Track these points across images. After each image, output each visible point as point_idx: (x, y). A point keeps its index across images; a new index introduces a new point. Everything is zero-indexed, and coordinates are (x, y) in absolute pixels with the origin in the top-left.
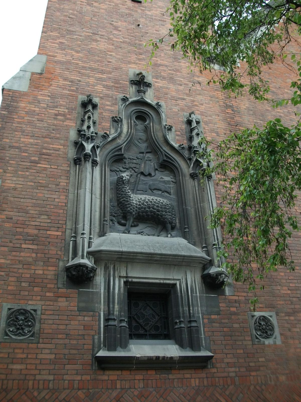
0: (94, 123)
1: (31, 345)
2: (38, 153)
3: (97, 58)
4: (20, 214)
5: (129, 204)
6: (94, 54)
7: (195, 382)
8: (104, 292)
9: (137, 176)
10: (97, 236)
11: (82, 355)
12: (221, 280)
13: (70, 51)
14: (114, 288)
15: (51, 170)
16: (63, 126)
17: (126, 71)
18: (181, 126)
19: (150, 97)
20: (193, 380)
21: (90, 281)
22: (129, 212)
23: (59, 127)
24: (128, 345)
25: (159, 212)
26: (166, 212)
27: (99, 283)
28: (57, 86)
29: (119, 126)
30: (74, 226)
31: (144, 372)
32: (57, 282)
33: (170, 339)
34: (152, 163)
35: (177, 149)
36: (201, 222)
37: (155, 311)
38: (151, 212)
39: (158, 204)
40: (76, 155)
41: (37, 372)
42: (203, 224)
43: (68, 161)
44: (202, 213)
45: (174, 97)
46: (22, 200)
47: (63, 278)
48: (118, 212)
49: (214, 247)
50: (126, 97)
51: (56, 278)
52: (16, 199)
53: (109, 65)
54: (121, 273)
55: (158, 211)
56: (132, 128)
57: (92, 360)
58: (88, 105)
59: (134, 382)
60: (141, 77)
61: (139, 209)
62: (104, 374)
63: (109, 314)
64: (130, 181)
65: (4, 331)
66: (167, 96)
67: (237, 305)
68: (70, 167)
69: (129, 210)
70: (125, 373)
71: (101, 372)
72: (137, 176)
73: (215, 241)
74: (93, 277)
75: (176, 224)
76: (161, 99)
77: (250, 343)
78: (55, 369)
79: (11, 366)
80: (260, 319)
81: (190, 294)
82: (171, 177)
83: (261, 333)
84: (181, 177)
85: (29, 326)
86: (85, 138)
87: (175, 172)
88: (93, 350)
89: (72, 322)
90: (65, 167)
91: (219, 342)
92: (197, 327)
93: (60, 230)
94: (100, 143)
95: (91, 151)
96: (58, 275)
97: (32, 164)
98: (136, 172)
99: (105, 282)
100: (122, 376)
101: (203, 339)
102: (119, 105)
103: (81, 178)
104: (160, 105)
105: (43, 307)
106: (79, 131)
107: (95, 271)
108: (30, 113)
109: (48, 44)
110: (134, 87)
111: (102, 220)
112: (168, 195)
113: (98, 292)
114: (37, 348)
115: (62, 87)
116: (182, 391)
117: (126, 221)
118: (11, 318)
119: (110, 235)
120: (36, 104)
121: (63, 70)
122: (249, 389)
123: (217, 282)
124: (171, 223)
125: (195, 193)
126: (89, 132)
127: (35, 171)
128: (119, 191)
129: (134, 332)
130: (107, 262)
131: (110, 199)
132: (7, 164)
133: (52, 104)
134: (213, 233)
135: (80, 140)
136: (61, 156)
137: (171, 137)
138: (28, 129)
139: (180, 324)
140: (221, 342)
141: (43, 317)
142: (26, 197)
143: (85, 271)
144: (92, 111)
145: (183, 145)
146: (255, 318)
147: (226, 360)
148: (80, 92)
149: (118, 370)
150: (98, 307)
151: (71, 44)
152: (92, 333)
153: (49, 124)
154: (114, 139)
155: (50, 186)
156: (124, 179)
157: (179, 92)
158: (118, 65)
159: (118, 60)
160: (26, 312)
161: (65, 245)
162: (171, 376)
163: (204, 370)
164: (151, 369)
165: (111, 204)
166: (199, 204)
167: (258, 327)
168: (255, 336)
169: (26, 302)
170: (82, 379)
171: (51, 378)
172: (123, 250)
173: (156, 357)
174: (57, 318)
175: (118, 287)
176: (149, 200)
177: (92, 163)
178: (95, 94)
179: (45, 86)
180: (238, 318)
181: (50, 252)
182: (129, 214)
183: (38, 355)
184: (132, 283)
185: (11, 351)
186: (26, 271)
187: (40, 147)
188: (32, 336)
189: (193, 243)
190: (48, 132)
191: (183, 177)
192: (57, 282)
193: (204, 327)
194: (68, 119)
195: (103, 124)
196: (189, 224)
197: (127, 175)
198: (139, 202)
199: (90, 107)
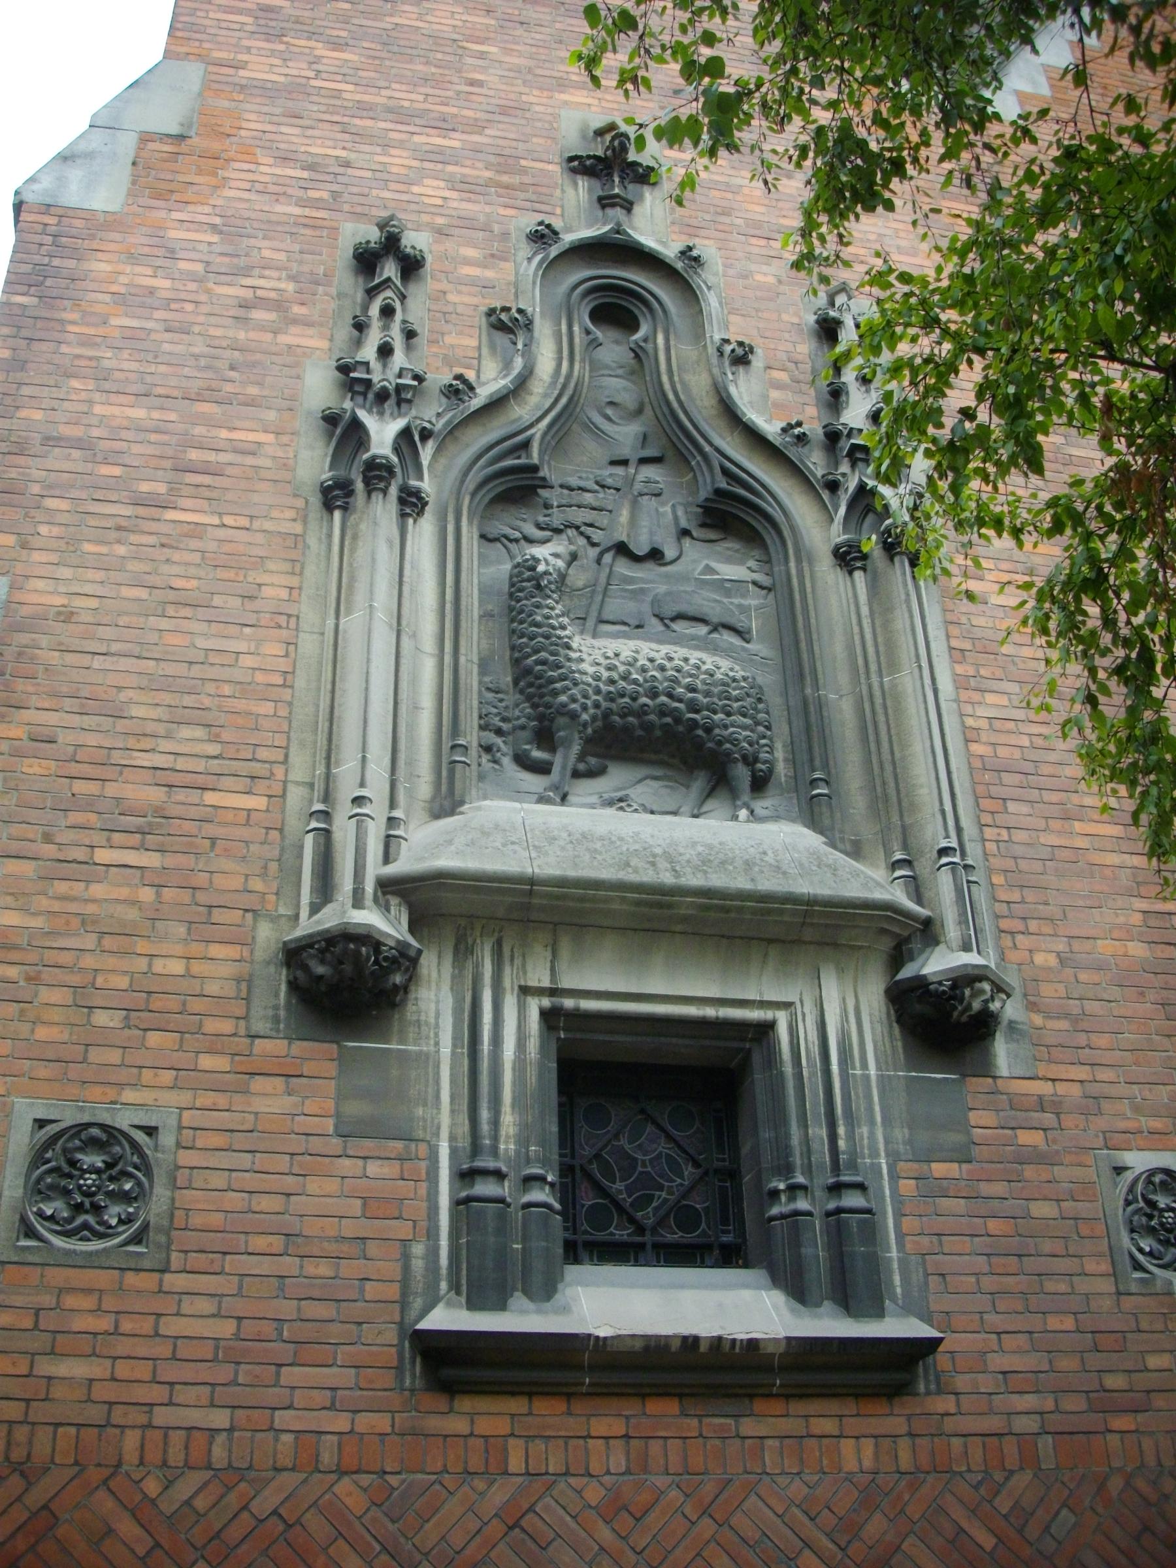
0: (410, 335)
1: (131, 1278)
2: (168, 464)
3: (420, 67)
4: (87, 721)
5: (563, 678)
6: (409, 51)
7: (859, 1451)
8: (453, 1053)
9: (598, 561)
10: (424, 816)
11: (353, 1327)
12: (976, 1005)
13: (303, 43)
14: (497, 1040)
15: (222, 533)
16: (274, 349)
17: (549, 118)
18: (790, 347)
19: (652, 225)
20: (847, 1445)
21: (393, 1005)
22: (562, 710)
23: (258, 356)
24: (560, 1286)
25: (697, 712)
26: (729, 714)
27: (432, 1014)
28: (247, 186)
29: (520, 346)
30: (320, 770)
31: (630, 1407)
32: (248, 1009)
33: (746, 1265)
34: (663, 504)
35: (777, 441)
36: (886, 756)
37: (679, 1146)
38: (663, 711)
39: (691, 676)
40: (330, 469)
41: (157, 1393)
42: (894, 763)
43: (295, 495)
44: (886, 714)
45: (757, 224)
46: (98, 662)
47: (276, 988)
48: (517, 713)
49: (944, 860)
50: (548, 226)
51: (244, 994)
52: (70, 658)
53: (474, 97)
54: (529, 975)
55: (694, 707)
56: (577, 358)
57: (400, 1345)
58: (385, 261)
59: (586, 1449)
60: (613, 139)
61: (610, 697)
62: (451, 1411)
63: (476, 1149)
64: (568, 581)
65: (18, 1217)
66: (726, 220)
67: (1048, 1118)
68: (305, 522)
69: (564, 705)
70: (542, 1406)
71: (442, 1402)
72: (598, 561)
73: (947, 837)
74: (406, 989)
75: (771, 764)
76: (702, 232)
77: (1107, 1286)
78: (234, 1383)
79: (46, 1367)
80: (1149, 1181)
81: (835, 1068)
82: (752, 563)
83: (1157, 1246)
84: (792, 564)
85: (126, 1198)
86: (370, 396)
87: (769, 542)
88: (404, 1304)
89: (313, 1185)
90: (284, 521)
91: (963, 1278)
92: (869, 1211)
93: (261, 787)
94: (434, 420)
95: (397, 449)
96: (250, 982)
97: (141, 511)
98: (594, 545)
99: (457, 1011)
100: (530, 1418)
101: (895, 1266)
102: (519, 259)
103: (351, 565)
104: (696, 259)
105: (186, 1114)
106: (344, 369)
107: (414, 961)
108: (137, 299)
109: (211, 15)
110: (583, 183)
111: (446, 746)
112: (736, 641)
113: (427, 1055)
114: (160, 1291)
115: (272, 188)
116: (797, 1489)
117: (553, 750)
118: (48, 1161)
119: (479, 808)
120: (159, 262)
121: (275, 119)
122: (1102, 1487)
123: (955, 1014)
124: (750, 761)
125: (856, 629)
126: (388, 371)
127: (152, 540)
128: (521, 622)
129: (586, 1232)
130: (463, 922)
131: (480, 659)
132: (33, 512)
133: (227, 260)
134: (937, 804)
135: (348, 405)
136: (264, 474)
137: (745, 392)
138: (126, 365)
139: (792, 1199)
140: (973, 1279)
141: (186, 1158)
142: (115, 647)
143: (368, 959)
144: (398, 283)
145: (799, 424)
146: (1129, 1176)
147: (998, 1361)
148: (346, 207)
149: (513, 1394)
150: (425, 1120)
151: (307, 14)
152: (402, 1230)
153: (213, 343)
154: (497, 404)
155: (217, 601)
156: (541, 568)
157: (780, 204)
158: (512, 96)
159: (511, 74)
160: (112, 1134)
161: (282, 849)
162: (748, 1426)
163: (896, 1400)
164: (663, 1392)
165: (487, 679)
166: (875, 679)
167: (1144, 1219)
168: (1127, 1257)
169: (111, 1093)
170: (357, 1429)
171: (220, 1419)
172: (537, 871)
173: (685, 1338)
174: (248, 1166)
175: (517, 1037)
176: (651, 660)
177: (402, 501)
178: (414, 217)
179: (195, 188)
180: (1051, 1178)
181: (218, 880)
182: (562, 721)
183: (163, 1319)
184: (580, 1018)
185: (48, 1300)
186: (111, 962)
187: (174, 440)
188: (137, 1239)
189: (848, 847)
190: (210, 374)
191: (805, 564)
192: (248, 1009)
193: (899, 1215)
194: (295, 321)
195: (449, 340)
196: (831, 762)
197: (556, 555)
198: (610, 668)
199: (390, 270)
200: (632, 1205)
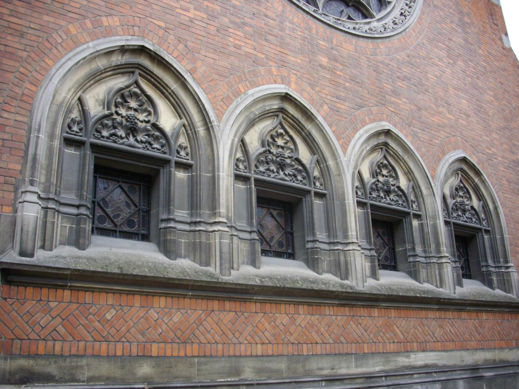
200: (113, 216)
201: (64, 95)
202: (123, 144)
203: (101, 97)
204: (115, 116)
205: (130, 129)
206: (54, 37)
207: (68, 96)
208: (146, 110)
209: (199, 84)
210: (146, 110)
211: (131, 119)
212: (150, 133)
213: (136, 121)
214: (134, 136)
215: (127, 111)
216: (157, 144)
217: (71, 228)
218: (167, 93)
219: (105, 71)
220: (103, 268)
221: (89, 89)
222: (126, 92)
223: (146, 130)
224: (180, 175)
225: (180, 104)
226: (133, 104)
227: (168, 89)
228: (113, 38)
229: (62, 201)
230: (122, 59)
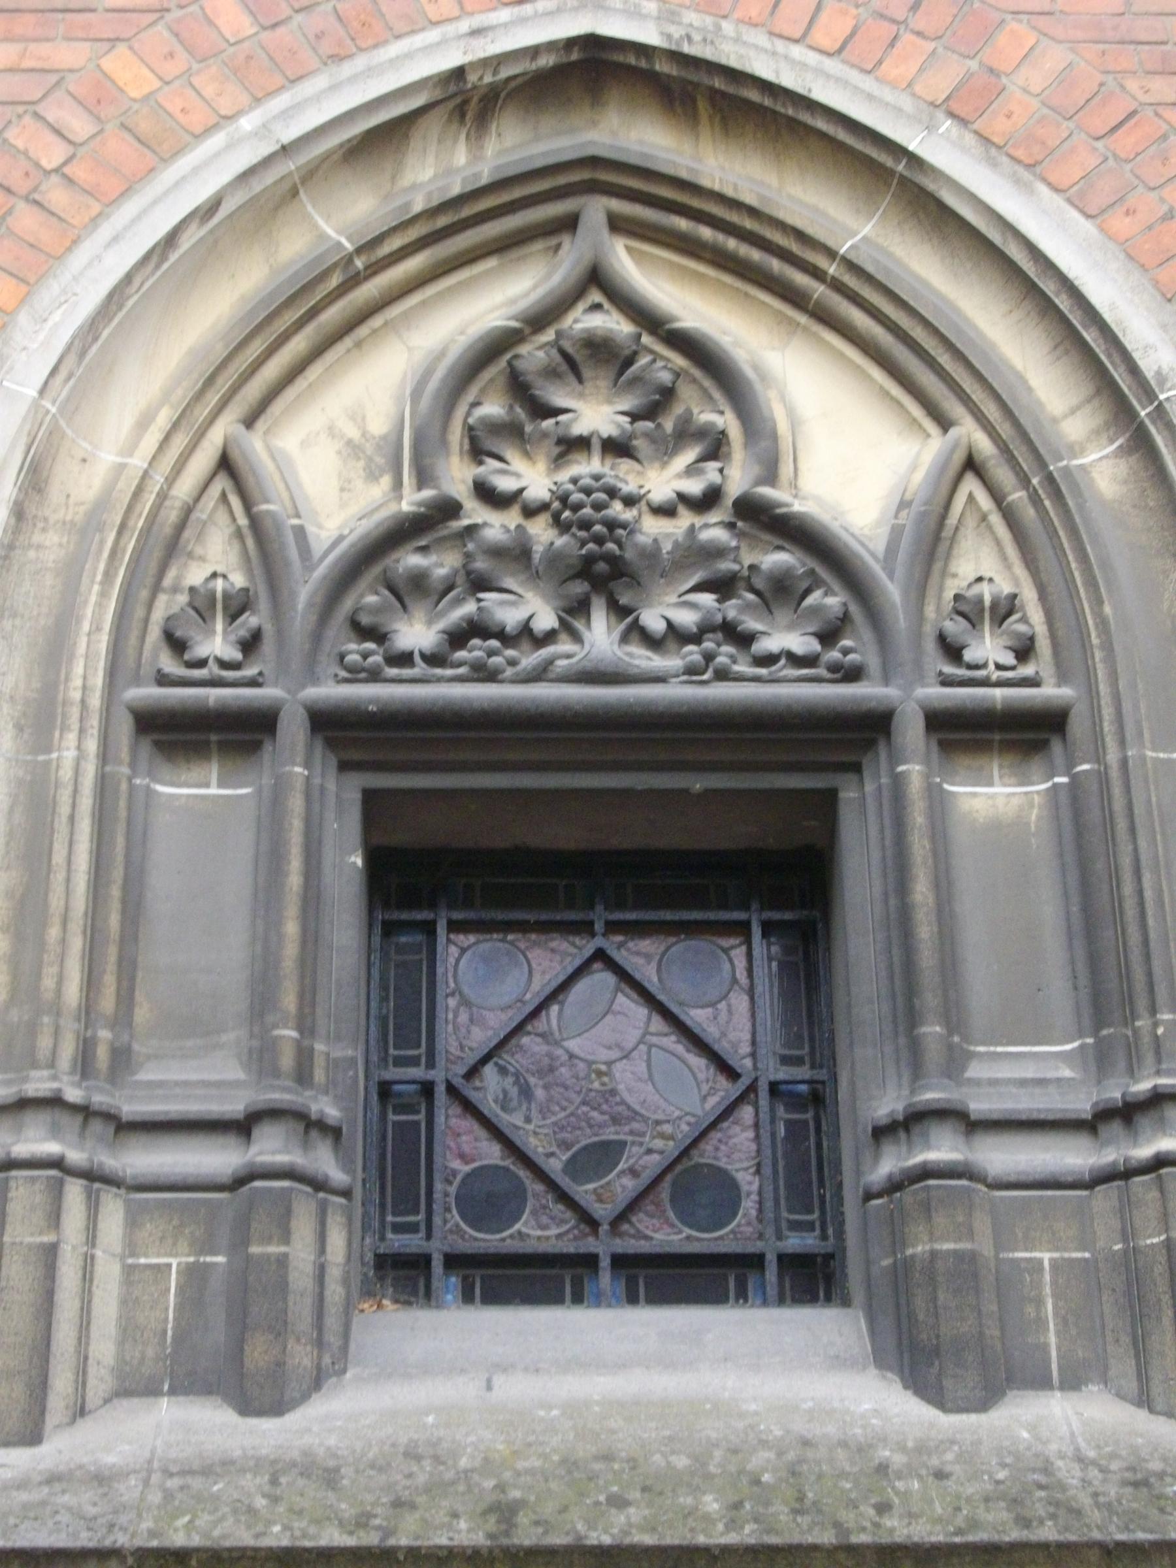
201: (108, 458)
202: (539, 675)
203: (379, 425)
204: (475, 513)
205: (585, 569)
206: (20, 144)
207: (139, 462)
208: (686, 433)
209: (1030, 164)
210: (686, 433)
211: (577, 507)
212: (726, 566)
213: (617, 509)
214: (620, 611)
215: (558, 462)
216: (791, 627)
217: (195, 1276)
218: (819, 290)
219: (372, 254)
220: (362, 1521)
221: (290, 393)
222: (534, 354)
223: (697, 553)
224: (996, 798)
225: (918, 333)
226: (596, 413)
227: (821, 261)
228: (395, 49)
229: (130, 1109)
230: (475, 158)
